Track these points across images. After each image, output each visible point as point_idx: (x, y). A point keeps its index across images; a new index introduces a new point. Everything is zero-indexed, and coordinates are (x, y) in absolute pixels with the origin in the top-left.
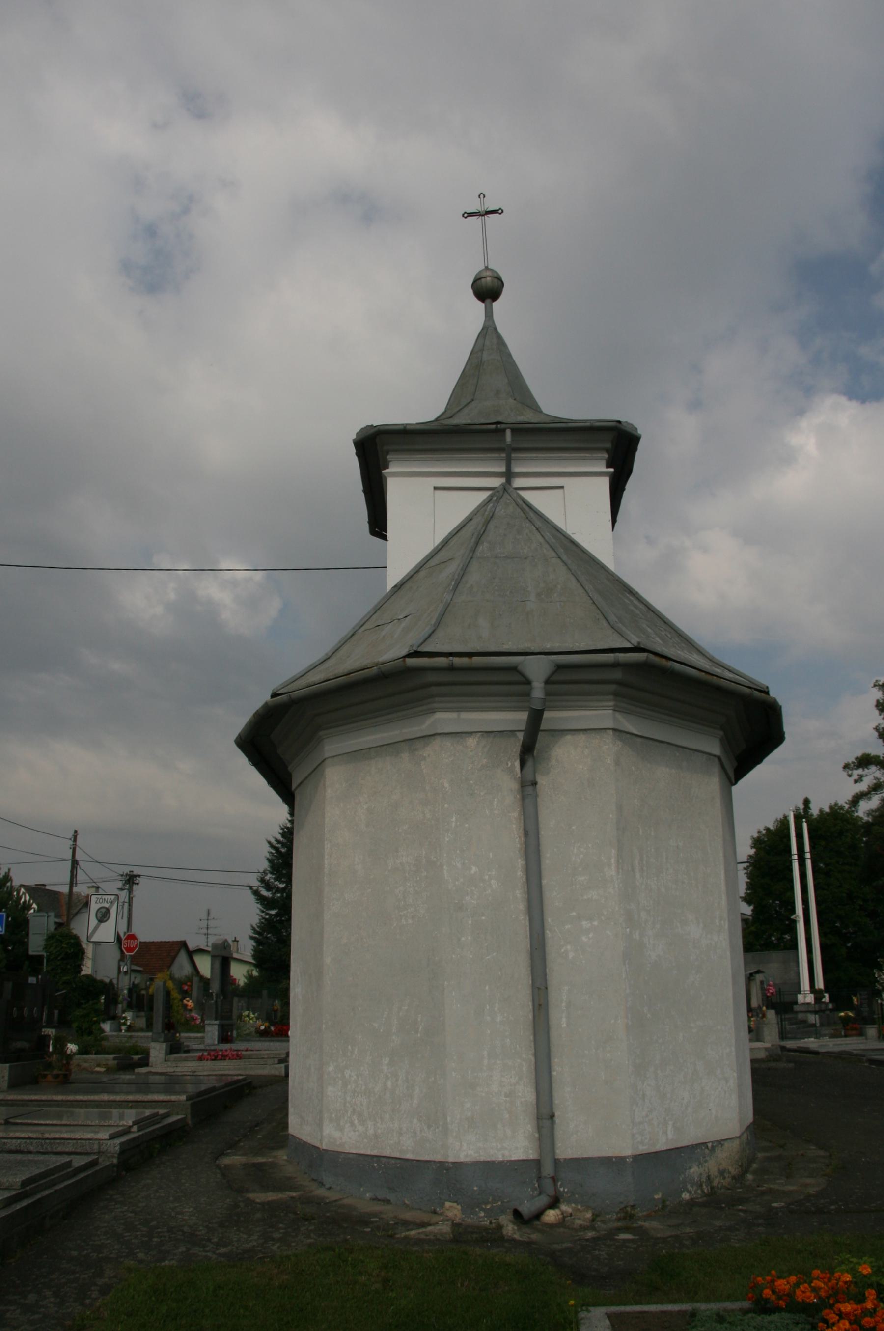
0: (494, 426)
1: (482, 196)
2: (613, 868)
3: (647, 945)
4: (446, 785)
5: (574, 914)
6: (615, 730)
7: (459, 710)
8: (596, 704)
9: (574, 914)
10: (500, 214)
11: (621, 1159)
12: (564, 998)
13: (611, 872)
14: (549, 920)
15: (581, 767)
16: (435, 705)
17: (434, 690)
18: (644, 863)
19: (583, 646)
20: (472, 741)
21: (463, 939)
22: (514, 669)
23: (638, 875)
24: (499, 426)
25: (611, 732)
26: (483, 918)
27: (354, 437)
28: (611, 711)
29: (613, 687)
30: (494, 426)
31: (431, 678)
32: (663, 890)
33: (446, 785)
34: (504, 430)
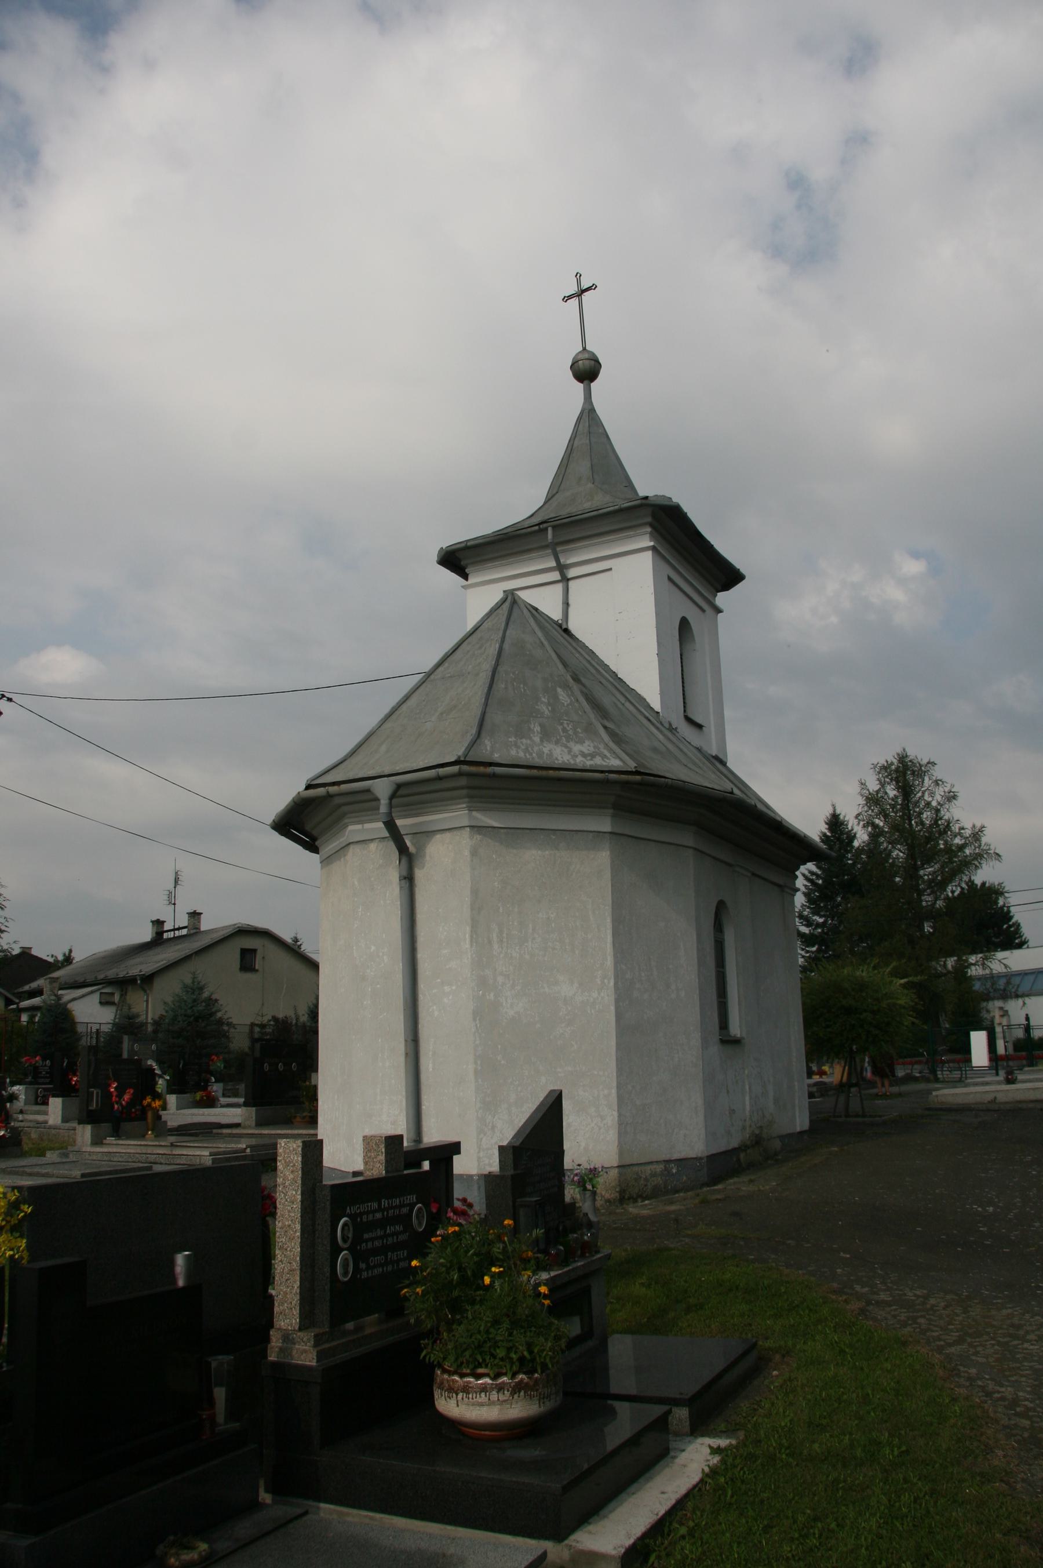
0: (537, 528)
1: (579, 275)
2: (467, 942)
3: (504, 1004)
4: (356, 883)
5: (439, 980)
6: (471, 827)
7: (362, 822)
8: (454, 807)
9: (439, 980)
10: (594, 289)
11: (471, 1176)
12: (431, 1048)
13: (466, 945)
14: (422, 986)
15: (447, 860)
16: (346, 821)
17: (345, 809)
18: (505, 935)
19: (422, 765)
20: (373, 846)
21: (365, 1003)
22: (368, 791)
23: (496, 946)
24: (541, 526)
25: (468, 829)
26: (378, 986)
27: (436, 559)
28: (467, 811)
29: (465, 792)
30: (537, 528)
31: (337, 801)
32: (527, 957)
33: (356, 883)
34: (546, 529)
